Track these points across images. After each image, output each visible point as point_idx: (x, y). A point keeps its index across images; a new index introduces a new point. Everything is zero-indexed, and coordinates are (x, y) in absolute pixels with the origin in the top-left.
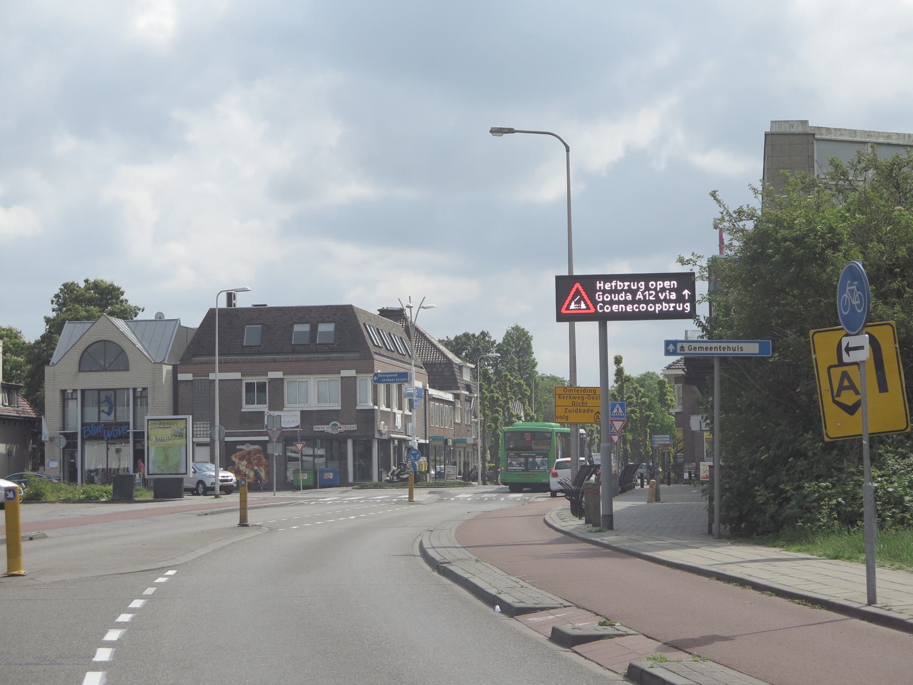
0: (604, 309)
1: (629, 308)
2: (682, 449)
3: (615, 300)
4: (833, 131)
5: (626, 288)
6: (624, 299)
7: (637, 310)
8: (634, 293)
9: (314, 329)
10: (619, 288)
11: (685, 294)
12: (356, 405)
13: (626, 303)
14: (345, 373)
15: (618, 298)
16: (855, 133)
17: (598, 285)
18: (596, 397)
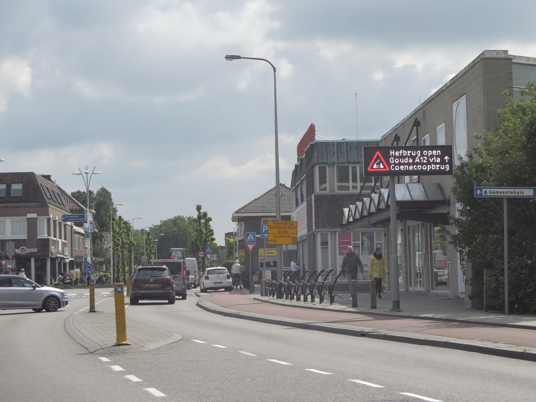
0: (395, 169)
1: (411, 168)
2: (244, 263)
3: (402, 162)
4: (517, 58)
5: (409, 155)
6: (407, 162)
7: (416, 169)
8: (414, 158)
9: (9, 187)
10: (404, 155)
11: (446, 159)
12: (37, 236)
13: (409, 164)
14: (29, 216)
15: (404, 161)
16: (529, 59)
17: (391, 153)
18: (293, 228)
